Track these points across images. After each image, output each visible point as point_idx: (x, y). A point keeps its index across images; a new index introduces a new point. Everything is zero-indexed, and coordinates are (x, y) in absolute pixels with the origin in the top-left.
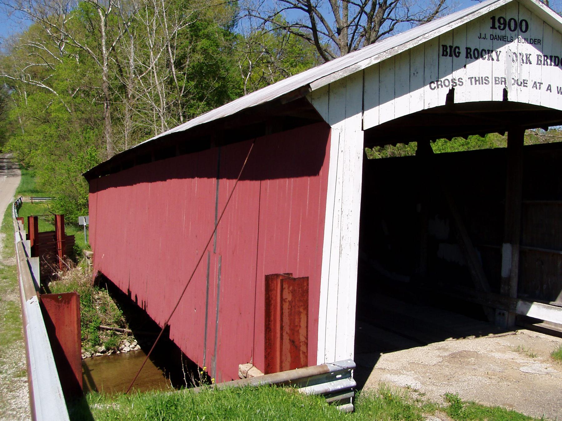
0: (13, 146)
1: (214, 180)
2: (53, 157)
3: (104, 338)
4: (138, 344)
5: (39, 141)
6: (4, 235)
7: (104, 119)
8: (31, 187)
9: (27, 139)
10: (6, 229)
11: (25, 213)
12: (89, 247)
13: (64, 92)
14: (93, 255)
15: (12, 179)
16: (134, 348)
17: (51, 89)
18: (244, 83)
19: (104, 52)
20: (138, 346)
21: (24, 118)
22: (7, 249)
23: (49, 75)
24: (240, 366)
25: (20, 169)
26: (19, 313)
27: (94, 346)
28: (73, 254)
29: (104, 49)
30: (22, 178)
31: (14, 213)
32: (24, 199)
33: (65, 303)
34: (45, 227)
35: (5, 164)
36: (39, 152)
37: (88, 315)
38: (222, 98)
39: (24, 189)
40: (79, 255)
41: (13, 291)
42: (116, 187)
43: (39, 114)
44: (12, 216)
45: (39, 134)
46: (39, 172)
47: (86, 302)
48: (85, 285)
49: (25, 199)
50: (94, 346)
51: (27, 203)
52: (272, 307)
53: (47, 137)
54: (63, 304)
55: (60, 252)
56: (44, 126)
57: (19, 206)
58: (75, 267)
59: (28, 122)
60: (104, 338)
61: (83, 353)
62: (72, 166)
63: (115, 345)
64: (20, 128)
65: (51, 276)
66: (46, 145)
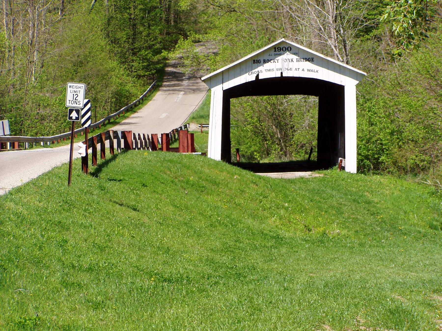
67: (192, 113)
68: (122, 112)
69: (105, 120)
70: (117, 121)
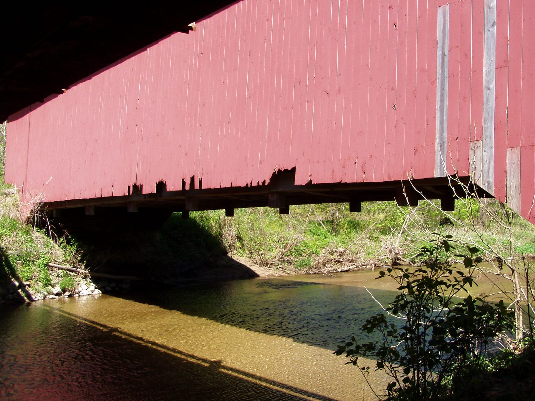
4: (96, 288)
20: (97, 291)
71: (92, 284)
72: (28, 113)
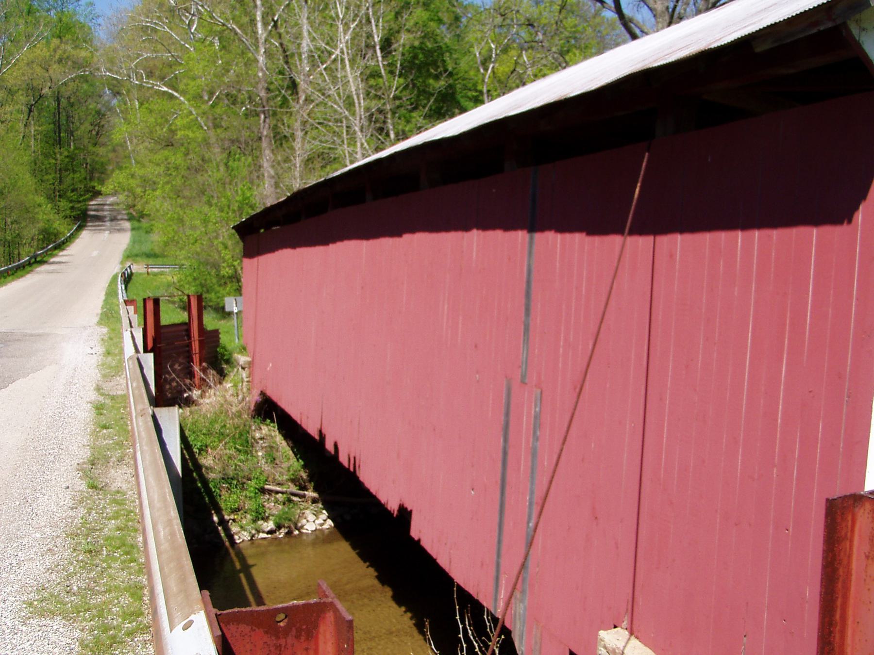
0: (119, 183)
1: (521, 235)
2: (181, 201)
3: (274, 507)
4: (328, 517)
5: (159, 175)
6: (105, 330)
7: (260, 138)
8: (146, 248)
9: (140, 172)
10: (108, 318)
11: (140, 293)
12: (245, 349)
13: (198, 97)
14: (251, 364)
15: (117, 236)
16: (322, 525)
17: (176, 94)
18: (483, 81)
19: (260, 32)
20: (330, 523)
21: (135, 141)
22: (110, 358)
23: (172, 73)
24: (602, 634)
25: (129, 220)
26: (136, 530)
27: (255, 521)
28: (217, 361)
29: (259, 25)
30: (133, 235)
31: (120, 292)
32: (135, 268)
33: (298, 637)
34: (171, 316)
35: (106, 213)
36: (158, 192)
37: (246, 467)
38: (447, 105)
39: (135, 252)
40: (228, 362)
41: (120, 460)
42: (294, 247)
43: (159, 132)
44: (117, 294)
45: (158, 165)
46: (158, 225)
47: (242, 445)
48: (239, 415)
49: (138, 268)
50: (255, 521)
51: (141, 274)
52: (840, 585)
53: (170, 169)
54: (290, 640)
55: (196, 358)
56: (166, 152)
57: (127, 279)
58: (220, 383)
59: (141, 147)
60: (274, 507)
61: (236, 534)
62: (214, 214)
63: (290, 520)
64: (129, 157)
65: (182, 398)
66: (168, 183)
67: (125, 251)
68: (51, 250)
69: (31, 258)
70: (45, 259)
71: (324, 511)
72: (383, 579)
